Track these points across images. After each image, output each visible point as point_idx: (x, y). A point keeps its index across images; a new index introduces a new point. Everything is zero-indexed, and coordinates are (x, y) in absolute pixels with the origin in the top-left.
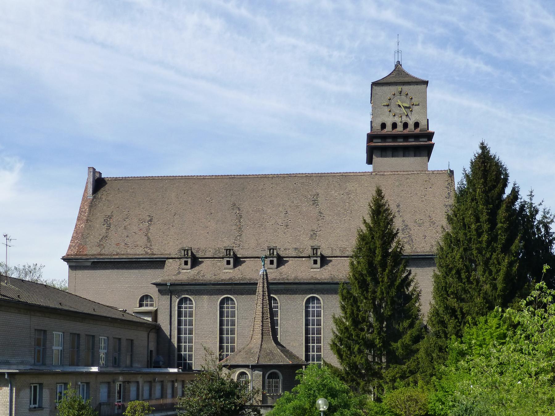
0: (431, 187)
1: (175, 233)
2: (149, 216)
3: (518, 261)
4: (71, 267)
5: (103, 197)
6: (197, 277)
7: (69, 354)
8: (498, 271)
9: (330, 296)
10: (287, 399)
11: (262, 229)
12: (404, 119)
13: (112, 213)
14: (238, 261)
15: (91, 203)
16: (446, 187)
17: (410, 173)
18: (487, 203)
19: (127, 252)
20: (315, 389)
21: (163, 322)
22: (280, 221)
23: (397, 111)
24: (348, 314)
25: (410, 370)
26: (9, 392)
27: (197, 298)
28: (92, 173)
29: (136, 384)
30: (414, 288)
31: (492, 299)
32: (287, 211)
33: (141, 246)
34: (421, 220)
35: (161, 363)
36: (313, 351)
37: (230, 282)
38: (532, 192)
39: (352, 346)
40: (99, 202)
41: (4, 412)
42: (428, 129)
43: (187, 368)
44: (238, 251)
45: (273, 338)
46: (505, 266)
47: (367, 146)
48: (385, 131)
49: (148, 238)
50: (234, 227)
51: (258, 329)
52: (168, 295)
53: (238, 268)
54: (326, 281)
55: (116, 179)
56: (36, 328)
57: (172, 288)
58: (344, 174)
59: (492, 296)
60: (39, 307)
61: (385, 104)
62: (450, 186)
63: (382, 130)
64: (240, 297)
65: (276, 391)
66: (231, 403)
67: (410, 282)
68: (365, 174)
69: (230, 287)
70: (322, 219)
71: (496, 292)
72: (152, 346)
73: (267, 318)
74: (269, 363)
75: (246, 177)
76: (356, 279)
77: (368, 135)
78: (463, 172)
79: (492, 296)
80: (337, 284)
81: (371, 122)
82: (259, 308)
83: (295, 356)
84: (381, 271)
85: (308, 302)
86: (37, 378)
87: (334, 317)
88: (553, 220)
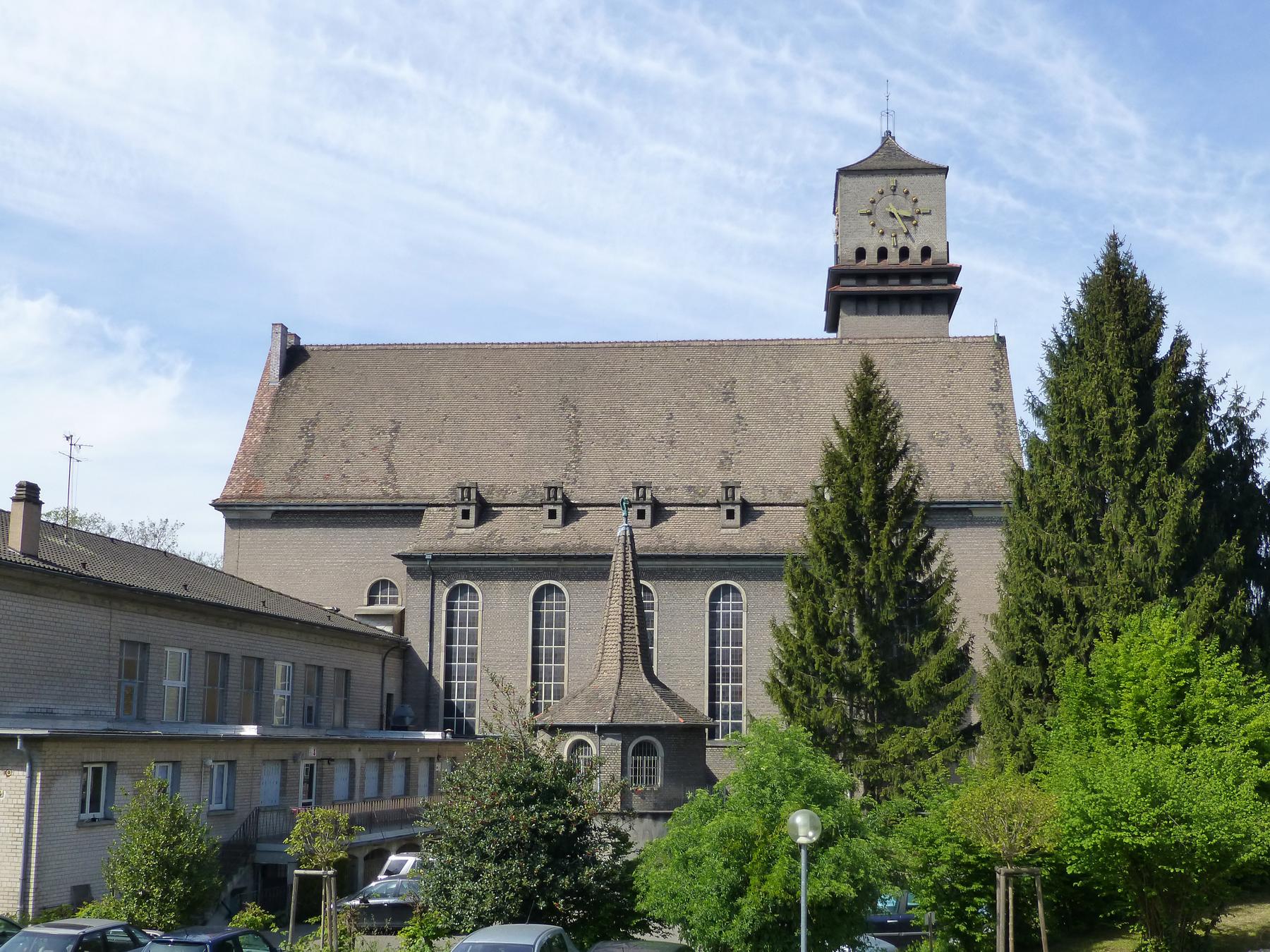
0: (960, 369)
1: (445, 455)
2: (392, 421)
3: (1203, 493)
4: (229, 522)
5: (301, 382)
6: (488, 543)
7: (201, 698)
8: (1161, 513)
9: (761, 584)
10: (701, 809)
11: (622, 449)
12: (902, 241)
13: (317, 415)
14: (571, 512)
15: (277, 395)
16: (991, 369)
17: (917, 341)
18: (1129, 363)
19: (345, 491)
20: (775, 782)
21: (416, 636)
22: (658, 434)
23: (888, 224)
24: (806, 618)
25: (938, 739)
26: (25, 781)
27: (487, 587)
28: (279, 335)
29: (280, 765)
30: (941, 564)
31: (1146, 578)
32: (671, 414)
33: (375, 481)
34: (943, 432)
35: (408, 721)
36: (726, 699)
37: (556, 553)
38: (1203, 356)
39: (812, 687)
40: (293, 392)
41: (12, 830)
42: (948, 262)
43: (463, 731)
44: (572, 492)
45: (644, 668)
46: (1179, 501)
47: (828, 293)
48: (864, 264)
49: (390, 465)
50: (564, 445)
51: (612, 651)
52: (427, 579)
53: (571, 525)
54: (752, 553)
55: (328, 349)
56: (122, 638)
57: (437, 565)
58: (785, 343)
59: (1147, 570)
60: (131, 590)
61: (865, 210)
62: (999, 366)
63: (857, 262)
64: (576, 585)
65: (650, 782)
66: (555, 816)
67: (934, 552)
68: (828, 342)
69: (555, 563)
70: (743, 429)
71: (1157, 561)
72: (392, 685)
73: (632, 628)
74: (636, 723)
75: (590, 345)
76: (821, 543)
77: (831, 271)
78: (1065, 306)
79: (1147, 570)
80: (781, 558)
81: (837, 247)
82: (616, 606)
83: (689, 707)
84: (874, 527)
85: (715, 595)
86: (100, 750)
87: (773, 625)
88: (1256, 411)
